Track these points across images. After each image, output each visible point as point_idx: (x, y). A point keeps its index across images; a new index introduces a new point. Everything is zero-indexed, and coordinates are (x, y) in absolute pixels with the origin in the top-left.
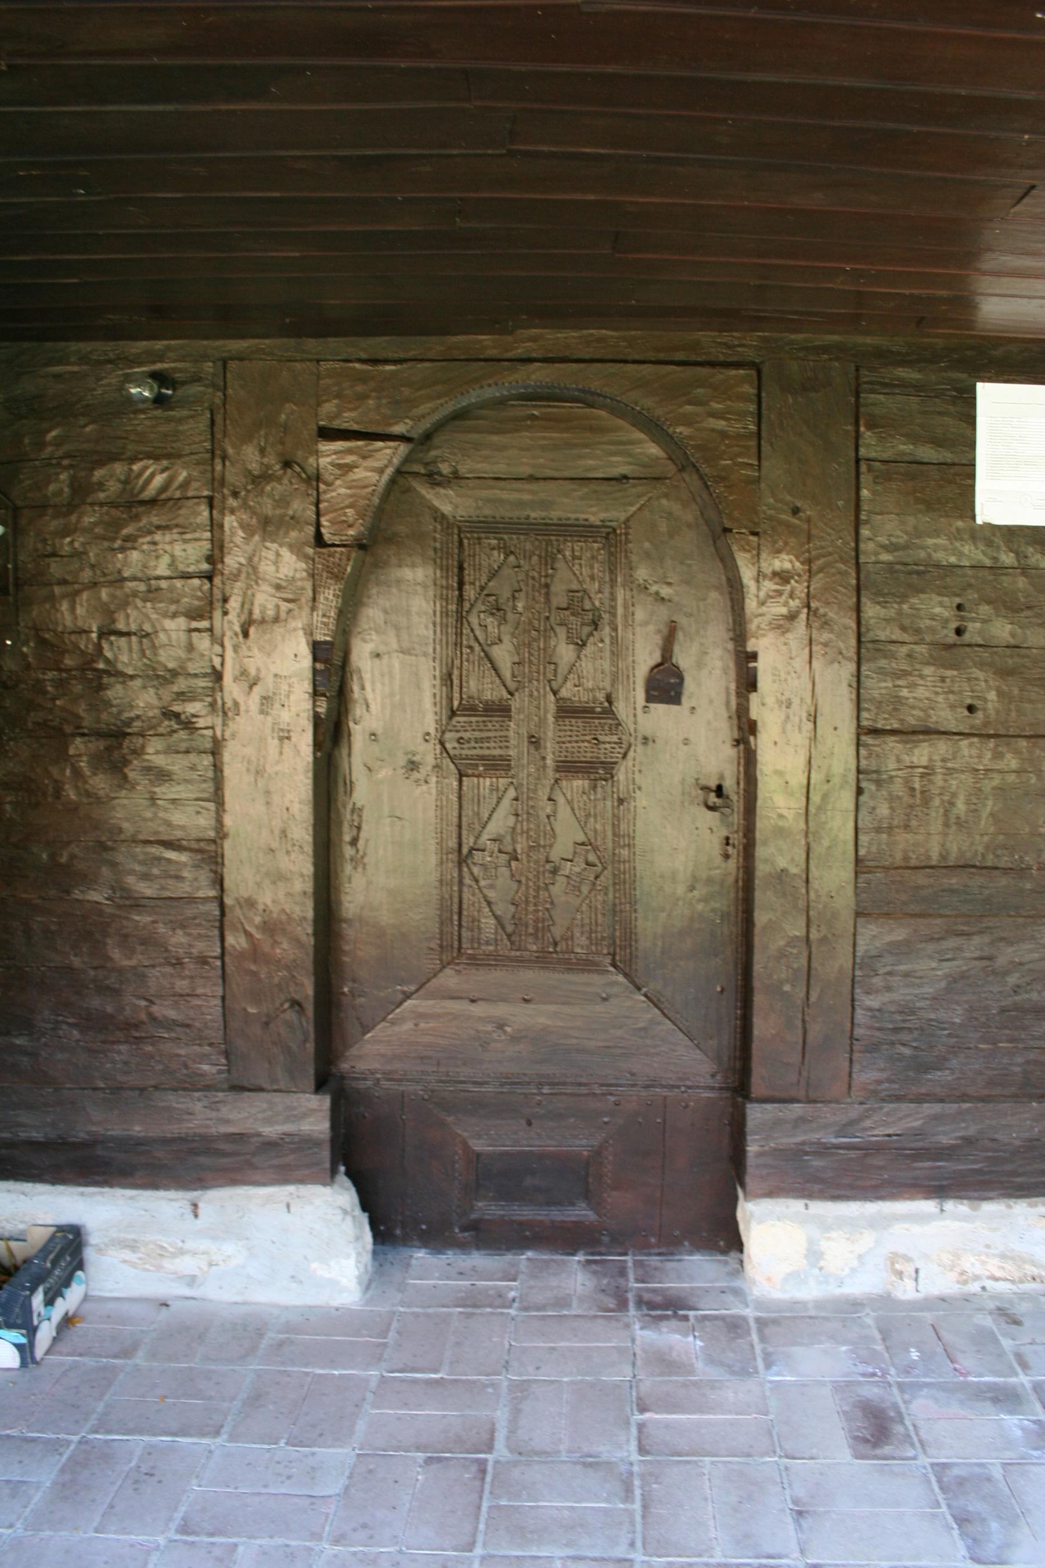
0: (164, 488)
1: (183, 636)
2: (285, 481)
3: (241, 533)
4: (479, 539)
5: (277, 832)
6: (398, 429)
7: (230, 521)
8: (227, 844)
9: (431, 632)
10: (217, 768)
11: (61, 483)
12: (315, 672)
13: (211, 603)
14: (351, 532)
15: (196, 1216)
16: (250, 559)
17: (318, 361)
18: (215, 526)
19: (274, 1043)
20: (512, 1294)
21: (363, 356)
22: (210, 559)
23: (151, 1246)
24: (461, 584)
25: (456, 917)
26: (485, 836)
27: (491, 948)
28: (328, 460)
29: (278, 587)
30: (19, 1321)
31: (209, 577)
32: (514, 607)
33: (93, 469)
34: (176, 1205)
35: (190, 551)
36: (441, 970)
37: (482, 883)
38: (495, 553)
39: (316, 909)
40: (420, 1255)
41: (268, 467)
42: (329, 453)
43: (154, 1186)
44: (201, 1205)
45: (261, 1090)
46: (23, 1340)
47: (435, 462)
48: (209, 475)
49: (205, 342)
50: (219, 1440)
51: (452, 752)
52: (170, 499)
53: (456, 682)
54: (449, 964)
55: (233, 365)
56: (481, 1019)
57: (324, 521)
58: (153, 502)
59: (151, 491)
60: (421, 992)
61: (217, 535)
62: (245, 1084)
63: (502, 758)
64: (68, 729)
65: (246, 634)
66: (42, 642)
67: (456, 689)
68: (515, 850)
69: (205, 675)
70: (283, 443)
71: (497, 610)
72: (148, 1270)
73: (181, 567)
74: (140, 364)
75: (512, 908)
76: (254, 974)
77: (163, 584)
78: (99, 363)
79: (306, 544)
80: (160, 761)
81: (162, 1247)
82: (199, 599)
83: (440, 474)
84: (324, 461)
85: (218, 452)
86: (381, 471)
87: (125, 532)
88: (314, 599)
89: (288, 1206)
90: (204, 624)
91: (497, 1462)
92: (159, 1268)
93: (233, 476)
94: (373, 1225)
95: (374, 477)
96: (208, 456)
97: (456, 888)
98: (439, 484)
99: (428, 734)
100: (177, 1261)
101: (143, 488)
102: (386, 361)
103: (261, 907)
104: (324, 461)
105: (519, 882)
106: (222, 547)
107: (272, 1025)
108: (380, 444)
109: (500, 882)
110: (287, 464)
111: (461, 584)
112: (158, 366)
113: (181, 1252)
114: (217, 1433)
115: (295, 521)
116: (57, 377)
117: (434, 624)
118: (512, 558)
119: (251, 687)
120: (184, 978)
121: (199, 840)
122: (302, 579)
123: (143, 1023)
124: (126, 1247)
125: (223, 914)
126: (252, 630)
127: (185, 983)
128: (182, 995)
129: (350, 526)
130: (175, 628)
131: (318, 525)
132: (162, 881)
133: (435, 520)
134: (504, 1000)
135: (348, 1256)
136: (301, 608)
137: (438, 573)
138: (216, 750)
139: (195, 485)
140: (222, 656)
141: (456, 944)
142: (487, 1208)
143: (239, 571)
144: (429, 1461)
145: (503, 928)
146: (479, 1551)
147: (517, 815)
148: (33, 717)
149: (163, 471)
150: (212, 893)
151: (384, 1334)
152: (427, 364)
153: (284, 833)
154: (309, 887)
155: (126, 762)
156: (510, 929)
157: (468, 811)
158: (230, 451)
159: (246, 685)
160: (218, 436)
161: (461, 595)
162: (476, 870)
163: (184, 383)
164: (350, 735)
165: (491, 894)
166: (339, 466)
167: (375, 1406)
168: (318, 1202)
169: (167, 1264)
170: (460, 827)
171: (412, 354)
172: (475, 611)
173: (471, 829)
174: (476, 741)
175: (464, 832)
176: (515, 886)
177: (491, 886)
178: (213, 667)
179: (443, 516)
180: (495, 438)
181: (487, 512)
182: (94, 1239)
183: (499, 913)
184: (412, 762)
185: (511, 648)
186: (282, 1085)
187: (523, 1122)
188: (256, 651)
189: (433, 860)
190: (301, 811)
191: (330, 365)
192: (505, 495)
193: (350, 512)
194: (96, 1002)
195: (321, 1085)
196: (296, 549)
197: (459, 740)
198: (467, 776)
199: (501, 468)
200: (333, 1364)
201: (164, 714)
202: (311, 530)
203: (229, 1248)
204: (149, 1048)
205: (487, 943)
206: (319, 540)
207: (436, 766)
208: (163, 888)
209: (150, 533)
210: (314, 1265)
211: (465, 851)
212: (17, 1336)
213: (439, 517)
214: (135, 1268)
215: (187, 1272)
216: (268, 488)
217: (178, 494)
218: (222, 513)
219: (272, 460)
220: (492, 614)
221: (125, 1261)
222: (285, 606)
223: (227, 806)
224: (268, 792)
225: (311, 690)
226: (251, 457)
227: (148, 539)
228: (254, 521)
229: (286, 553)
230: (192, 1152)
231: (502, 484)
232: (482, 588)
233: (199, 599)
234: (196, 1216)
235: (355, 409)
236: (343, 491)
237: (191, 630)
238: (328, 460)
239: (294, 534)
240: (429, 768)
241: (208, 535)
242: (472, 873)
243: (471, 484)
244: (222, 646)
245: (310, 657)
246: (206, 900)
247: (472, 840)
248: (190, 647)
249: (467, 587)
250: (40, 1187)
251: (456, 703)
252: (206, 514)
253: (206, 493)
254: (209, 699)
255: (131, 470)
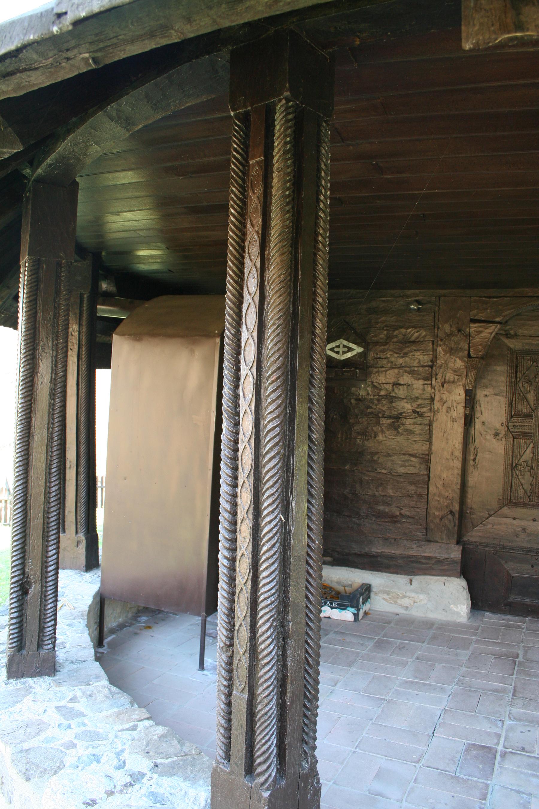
0: (417, 338)
1: (421, 387)
2: (458, 336)
3: (443, 353)
4: (523, 357)
5: (450, 453)
6: (498, 319)
7: (439, 349)
8: (432, 456)
9: (505, 388)
10: (430, 431)
11: (383, 335)
12: (466, 399)
13: (432, 376)
14: (480, 353)
15: (411, 584)
16: (446, 362)
17: (471, 297)
18: (434, 350)
19: (443, 526)
20: (523, 627)
21: (486, 295)
22: (432, 361)
23: (394, 594)
24: (516, 372)
25: (509, 488)
26: (521, 460)
27: (522, 500)
28: (473, 329)
29: (455, 371)
30: (355, 606)
31: (431, 367)
32: (535, 381)
33: (394, 331)
34: (404, 580)
35: (425, 358)
36: (503, 507)
37: (520, 477)
38: (529, 362)
39: (461, 480)
40: (488, 614)
41: (453, 331)
42: (474, 328)
43: (397, 573)
44: (413, 580)
45: (437, 542)
46: (356, 612)
47: (508, 330)
48: (433, 334)
49: (432, 291)
50: (424, 644)
51: (511, 430)
52: (419, 341)
53: (513, 406)
54: (506, 505)
55: (442, 298)
56: (517, 526)
57: (471, 350)
58: (414, 342)
59: (413, 338)
60: (496, 514)
61: (435, 353)
62: (432, 539)
63: (529, 433)
64: (380, 415)
65: (443, 386)
66: (374, 387)
67: (513, 408)
68: (532, 466)
69: (428, 399)
70: (458, 324)
71: (529, 381)
72: (392, 603)
73: (422, 363)
74: (411, 297)
75: (530, 487)
76: (438, 501)
77: (416, 369)
78: (398, 297)
79: (465, 357)
80: (411, 427)
81: (398, 595)
82: (428, 374)
83: (510, 334)
84: (472, 330)
85: (436, 326)
86: (491, 333)
87: (405, 351)
88: (467, 375)
89: (444, 584)
90: (429, 382)
91: (519, 661)
92: (396, 602)
93: (441, 334)
94: (472, 599)
95: (489, 335)
96: (433, 327)
97: (510, 478)
98: (509, 338)
99: (503, 423)
100: (403, 600)
101: (410, 338)
102: (494, 297)
103: (442, 478)
104: (472, 330)
105: (533, 477)
106: (436, 357)
107: (443, 519)
108: (491, 325)
109: (526, 477)
110: (459, 331)
111: (516, 372)
112: (417, 298)
113: (405, 597)
114: (423, 642)
115: (461, 349)
116: (384, 301)
117: (507, 385)
118: (535, 364)
119: (444, 404)
120: (413, 501)
121: (422, 454)
122: (463, 369)
123: (398, 516)
124: (385, 593)
125: (429, 480)
126: (445, 385)
127: (414, 503)
128: (412, 507)
129: (480, 351)
130: (418, 384)
131: (469, 351)
132: (409, 468)
133: (508, 350)
134: (526, 520)
135: (464, 605)
136: (462, 378)
137: (509, 368)
138: (430, 425)
139: (428, 337)
140: (434, 393)
141: (509, 498)
142: (514, 598)
143: (442, 366)
144: (495, 658)
145: (526, 493)
146: (514, 676)
147: (533, 453)
148: (369, 411)
149: (417, 332)
150: (425, 473)
151: (477, 630)
152: (508, 298)
153: (452, 454)
154: (460, 472)
155: (399, 427)
156: (529, 494)
157: (516, 451)
158: (440, 326)
159: (442, 403)
160: (436, 321)
161: (516, 376)
162: (517, 472)
163: (425, 304)
164: (475, 422)
165: (523, 481)
166: (477, 332)
167: (475, 644)
168: (455, 583)
169: (399, 601)
170: (513, 456)
171: (502, 295)
172: (521, 381)
173: (516, 457)
174: (522, 426)
175: (514, 458)
176: (531, 479)
177: (523, 478)
178: (431, 397)
179: (511, 348)
180: (530, 322)
181: (527, 347)
182: (374, 589)
183: (525, 488)
184: (496, 433)
185: (534, 395)
186: (444, 541)
187: (530, 566)
188: (446, 392)
189: (502, 467)
190: (459, 446)
191: (475, 298)
192: (534, 342)
193: (480, 347)
194: (381, 508)
195: (458, 543)
196: (461, 359)
197: (514, 426)
198: (516, 438)
199: (532, 333)
200: (459, 634)
201: (413, 412)
202: (466, 353)
203: (422, 597)
204: (399, 525)
205: (521, 498)
206: (469, 356)
207: (505, 435)
208: (409, 470)
209: (412, 352)
210: (452, 606)
211: (514, 465)
212: (354, 610)
213: (509, 349)
214: (387, 602)
215: (405, 605)
216: (453, 338)
217: (422, 340)
218: (437, 346)
219: (454, 329)
220: (527, 383)
221: (384, 599)
222: (456, 377)
223: (433, 443)
224: (447, 439)
225: (464, 405)
226: (447, 327)
227: (412, 354)
228: (447, 349)
229: (458, 360)
230: (412, 562)
231: (532, 338)
232: (524, 374)
233: (428, 374)
234: (411, 584)
235: (483, 313)
236: (478, 340)
237: (424, 384)
238: (473, 329)
239: (460, 354)
240: (503, 435)
241: (432, 353)
242: (516, 473)
243: (521, 338)
244: (435, 390)
245: (464, 395)
246: (423, 475)
247: (517, 461)
248: (424, 390)
249: (518, 373)
250: (357, 570)
251: (513, 413)
252: (431, 346)
253: (432, 339)
254: (429, 407)
255: (406, 331)
